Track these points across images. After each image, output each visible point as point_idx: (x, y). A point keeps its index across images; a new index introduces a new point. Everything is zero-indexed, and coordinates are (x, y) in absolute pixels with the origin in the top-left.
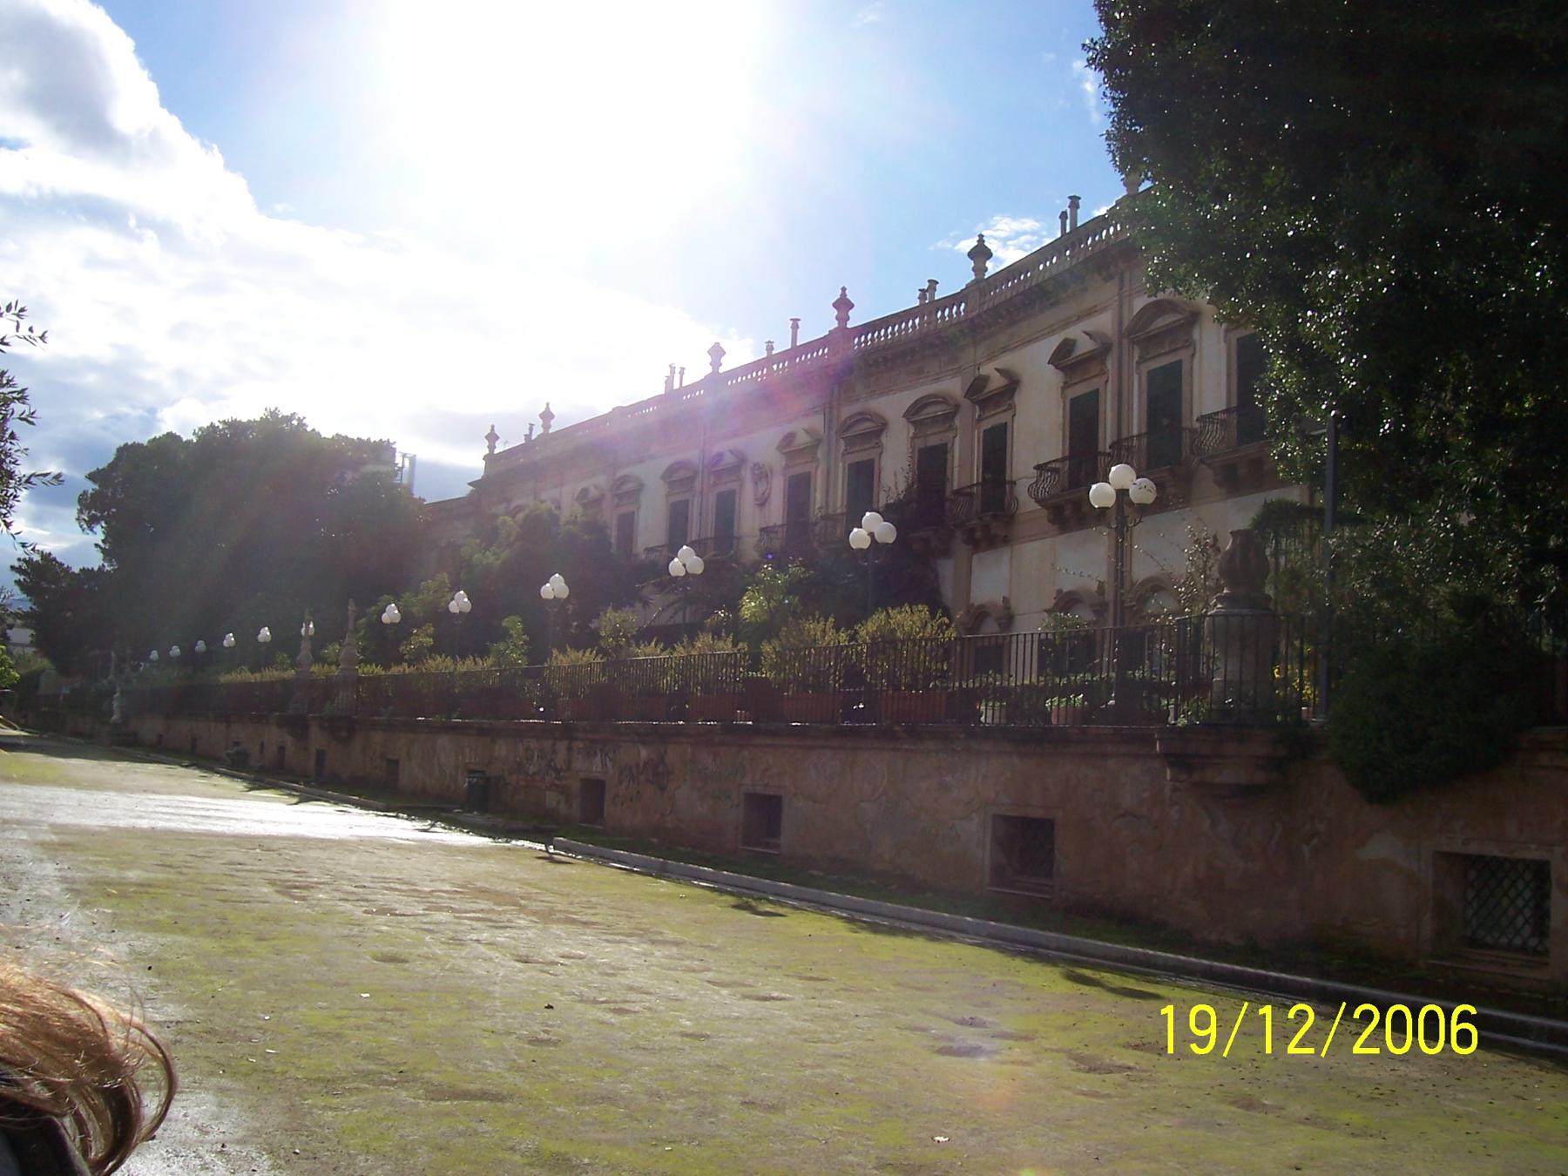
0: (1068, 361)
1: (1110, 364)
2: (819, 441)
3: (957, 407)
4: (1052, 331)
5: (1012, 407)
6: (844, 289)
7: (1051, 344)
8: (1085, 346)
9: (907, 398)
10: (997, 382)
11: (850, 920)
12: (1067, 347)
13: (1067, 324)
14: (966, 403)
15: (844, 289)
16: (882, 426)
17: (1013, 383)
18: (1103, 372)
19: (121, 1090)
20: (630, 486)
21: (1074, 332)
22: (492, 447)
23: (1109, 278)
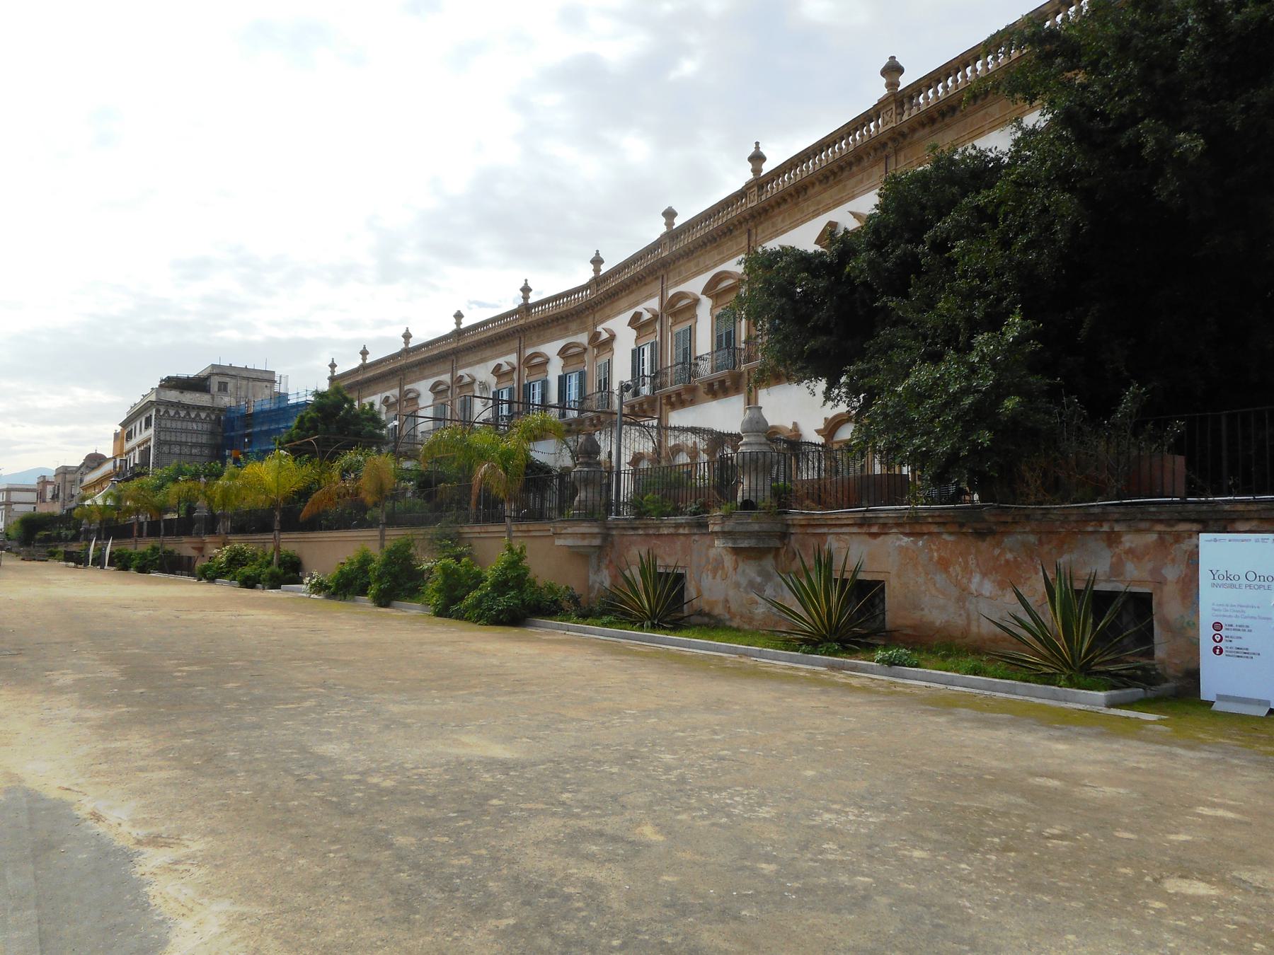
0: (637, 324)
1: (515, 376)
2: (514, 369)
3: (585, 349)
4: (630, 307)
5: (612, 350)
6: (757, 143)
7: (628, 315)
8: (506, 368)
9: (559, 344)
10: (605, 336)
11: (122, 563)
12: (637, 316)
13: (637, 304)
14: (590, 348)
15: (757, 143)
16: (547, 361)
17: (613, 337)
18: (655, 331)
19: (1141, 604)
20: (411, 395)
21: (639, 309)
22: (333, 372)
23: (657, 278)
